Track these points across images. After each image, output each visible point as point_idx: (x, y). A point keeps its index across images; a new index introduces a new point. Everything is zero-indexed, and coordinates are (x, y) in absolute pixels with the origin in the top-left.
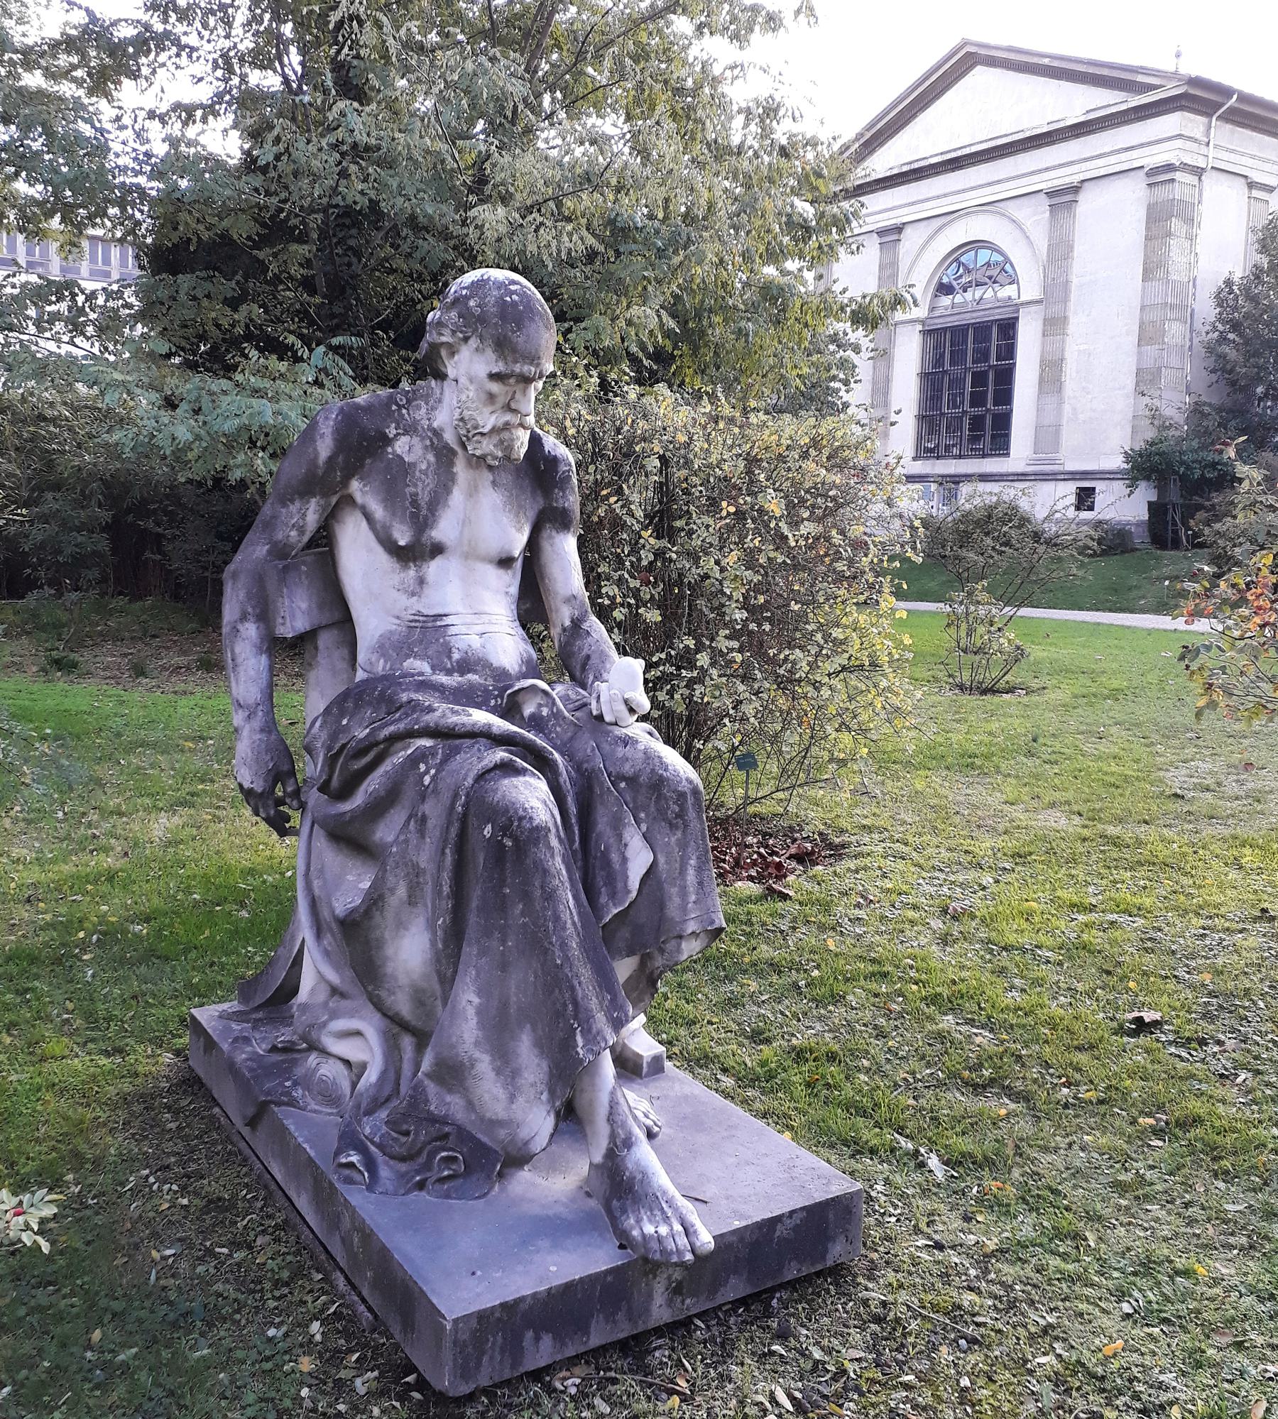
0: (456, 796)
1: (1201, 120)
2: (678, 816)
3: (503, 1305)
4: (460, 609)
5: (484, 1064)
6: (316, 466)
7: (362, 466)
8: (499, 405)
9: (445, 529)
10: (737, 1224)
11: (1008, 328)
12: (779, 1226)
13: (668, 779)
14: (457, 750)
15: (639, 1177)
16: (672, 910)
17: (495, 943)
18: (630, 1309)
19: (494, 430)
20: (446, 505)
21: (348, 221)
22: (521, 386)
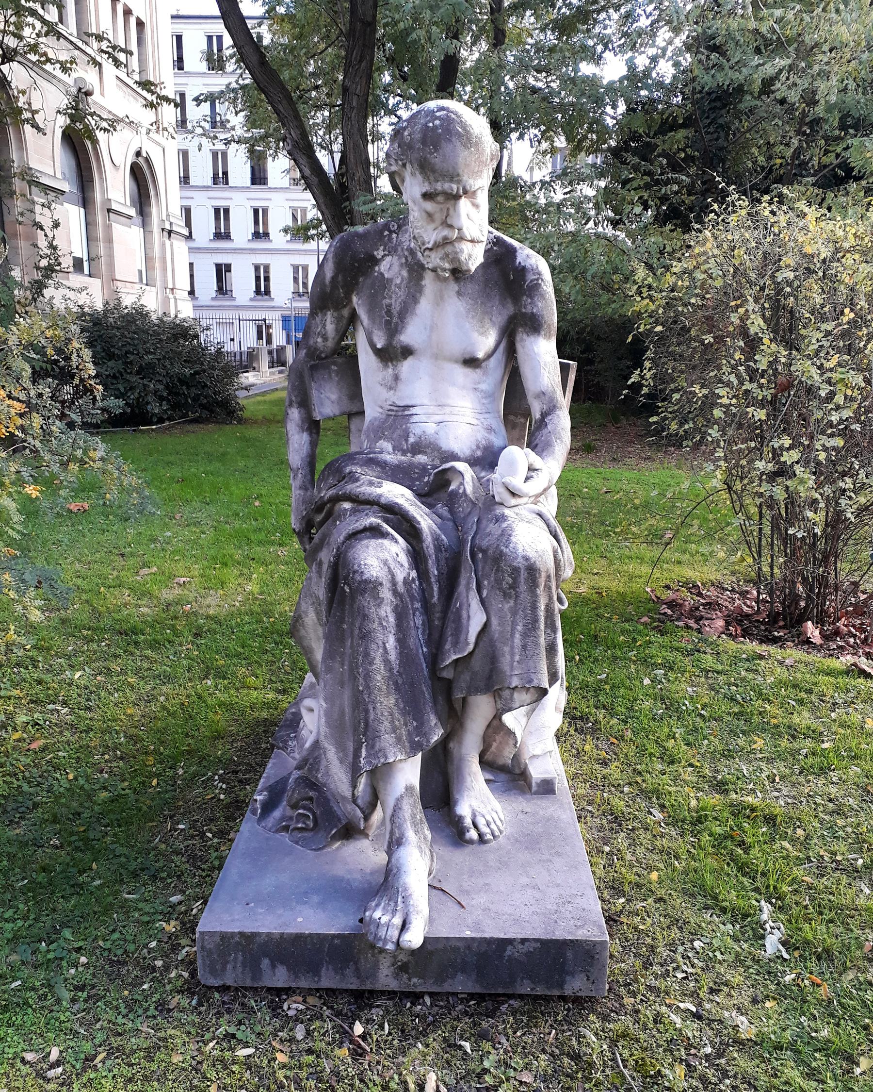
4: (426, 402)
6: (324, 283)
7: (357, 283)
8: (438, 222)
9: (412, 334)
10: (468, 934)
12: (509, 948)
13: (506, 554)
15: (395, 871)
16: (505, 662)
17: (337, 665)
18: (357, 970)
19: (437, 246)
20: (413, 313)
21: (718, 104)
22: (453, 202)
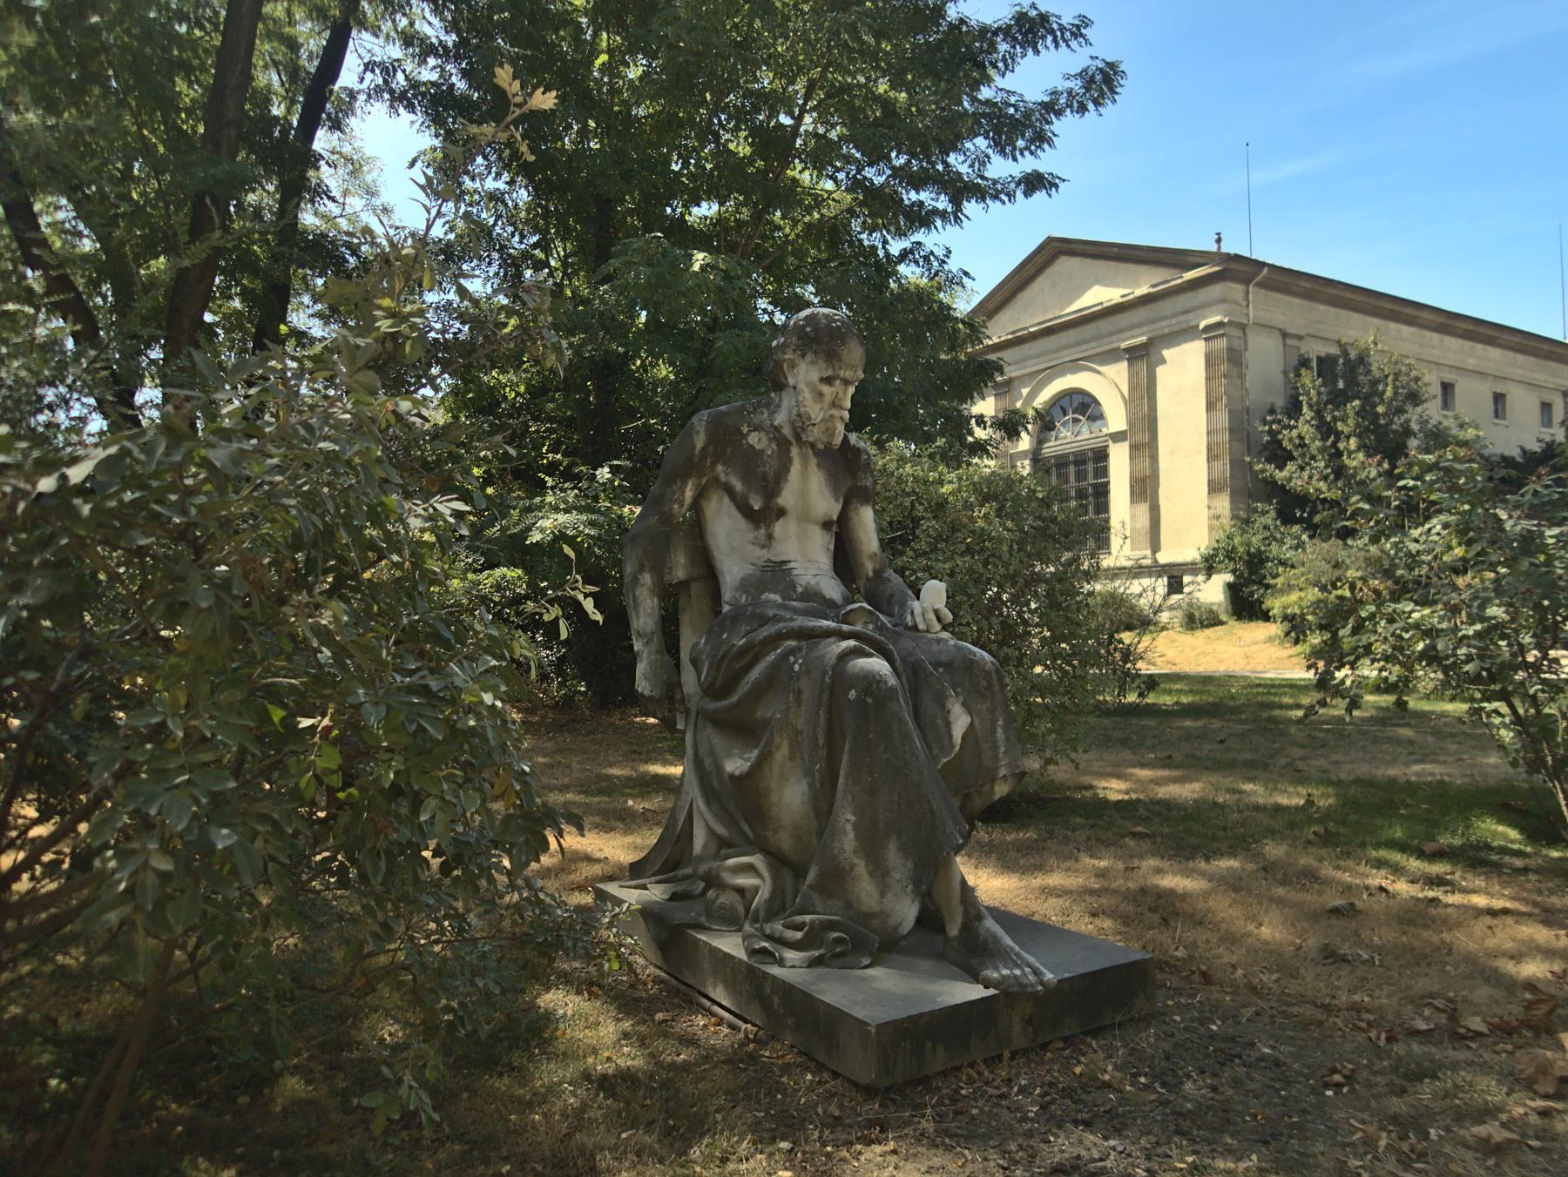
0: (824, 672)
1: (1240, 287)
2: (987, 689)
3: (909, 1017)
5: (861, 868)
11: (1101, 455)
14: (817, 644)
20: (786, 480)
